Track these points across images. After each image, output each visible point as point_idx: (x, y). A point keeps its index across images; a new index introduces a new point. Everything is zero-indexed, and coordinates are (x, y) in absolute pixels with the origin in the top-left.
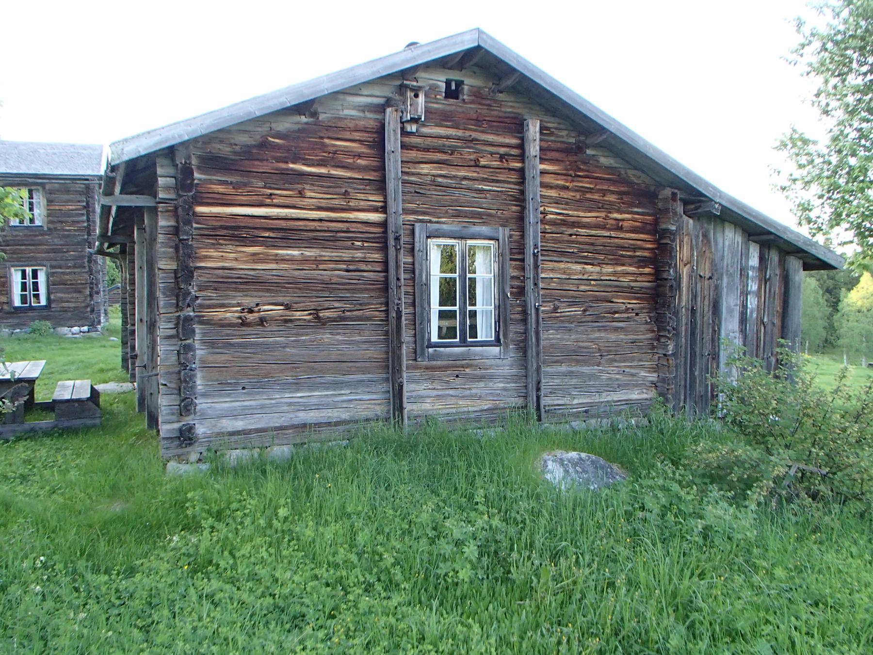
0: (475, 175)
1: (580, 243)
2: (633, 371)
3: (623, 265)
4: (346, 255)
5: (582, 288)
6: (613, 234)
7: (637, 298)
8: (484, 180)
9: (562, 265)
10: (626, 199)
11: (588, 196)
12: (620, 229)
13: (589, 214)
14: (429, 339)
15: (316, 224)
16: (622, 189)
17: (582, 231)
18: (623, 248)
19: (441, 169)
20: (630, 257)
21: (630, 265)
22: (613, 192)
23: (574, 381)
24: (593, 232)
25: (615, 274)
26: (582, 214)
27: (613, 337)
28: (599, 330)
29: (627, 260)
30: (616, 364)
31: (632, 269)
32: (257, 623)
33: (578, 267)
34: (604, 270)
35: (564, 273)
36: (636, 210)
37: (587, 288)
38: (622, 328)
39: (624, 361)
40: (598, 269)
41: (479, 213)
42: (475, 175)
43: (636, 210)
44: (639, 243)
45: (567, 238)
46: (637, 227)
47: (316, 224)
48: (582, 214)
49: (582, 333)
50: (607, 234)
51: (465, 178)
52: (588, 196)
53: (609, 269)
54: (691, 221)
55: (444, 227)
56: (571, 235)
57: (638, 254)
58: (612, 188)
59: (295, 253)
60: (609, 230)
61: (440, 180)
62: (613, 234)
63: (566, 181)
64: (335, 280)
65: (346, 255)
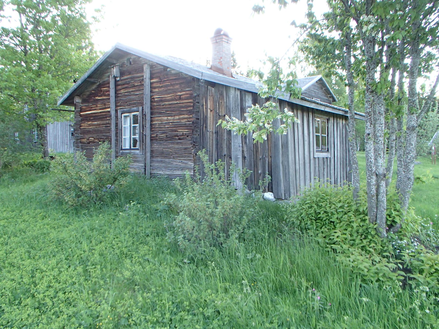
0: (134, 89)
1: (167, 108)
2: (185, 161)
3: (184, 115)
4: (105, 122)
5: (167, 126)
6: (178, 102)
7: (188, 129)
8: (137, 90)
9: (160, 118)
10: (183, 86)
11: (169, 88)
12: (180, 99)
13: (169, 96)
14: (122, 147)
15: (342, 165)
16: (181, 82)
17: (167, 103)
18: (182, 107)
19: (126, 90)
20: (185, 111)
21: (187, 114)
22: (177, 84)
23: (163, 165)
24: (171, 103)
25: (179, 119)
26: (166, 96)
27: (176, 146)
28: (171, 144)
29: (185, 112)
30: (179, 158)
31: (186, 116)
32: (339, 290)
33: (166, 118)
34: (175, 118)
35: (161, 121)
36: (187, 89)
37: (168, 126)
38: (180, 143)
39: (182, 157)
40: (173, 118)
41: (135, 103)
42: (134, 89)
43: (187, 89)
44: (189, 104)
45: (162, 107)
46: (188, 97)
47: (342, 165)
48: (166, 96)
49: (165, 145)
50: (176, 102)
51: (132, 91)
52: (169, 88)
53: (177, 117)
54: (213, 89)
55: (125, 109)
56: (163, 105)
57: (189, 109)
58: (177, 82)
59: (96, 123)
60: (176, 100)
61: (126, 94)
62: (178, 102)
63: (160, 84)
64: (102, 130)
65: (105, 122)
